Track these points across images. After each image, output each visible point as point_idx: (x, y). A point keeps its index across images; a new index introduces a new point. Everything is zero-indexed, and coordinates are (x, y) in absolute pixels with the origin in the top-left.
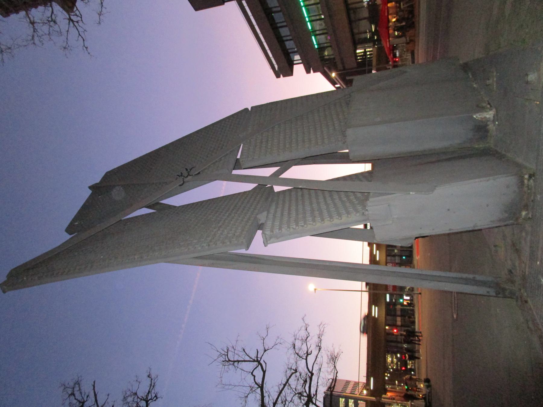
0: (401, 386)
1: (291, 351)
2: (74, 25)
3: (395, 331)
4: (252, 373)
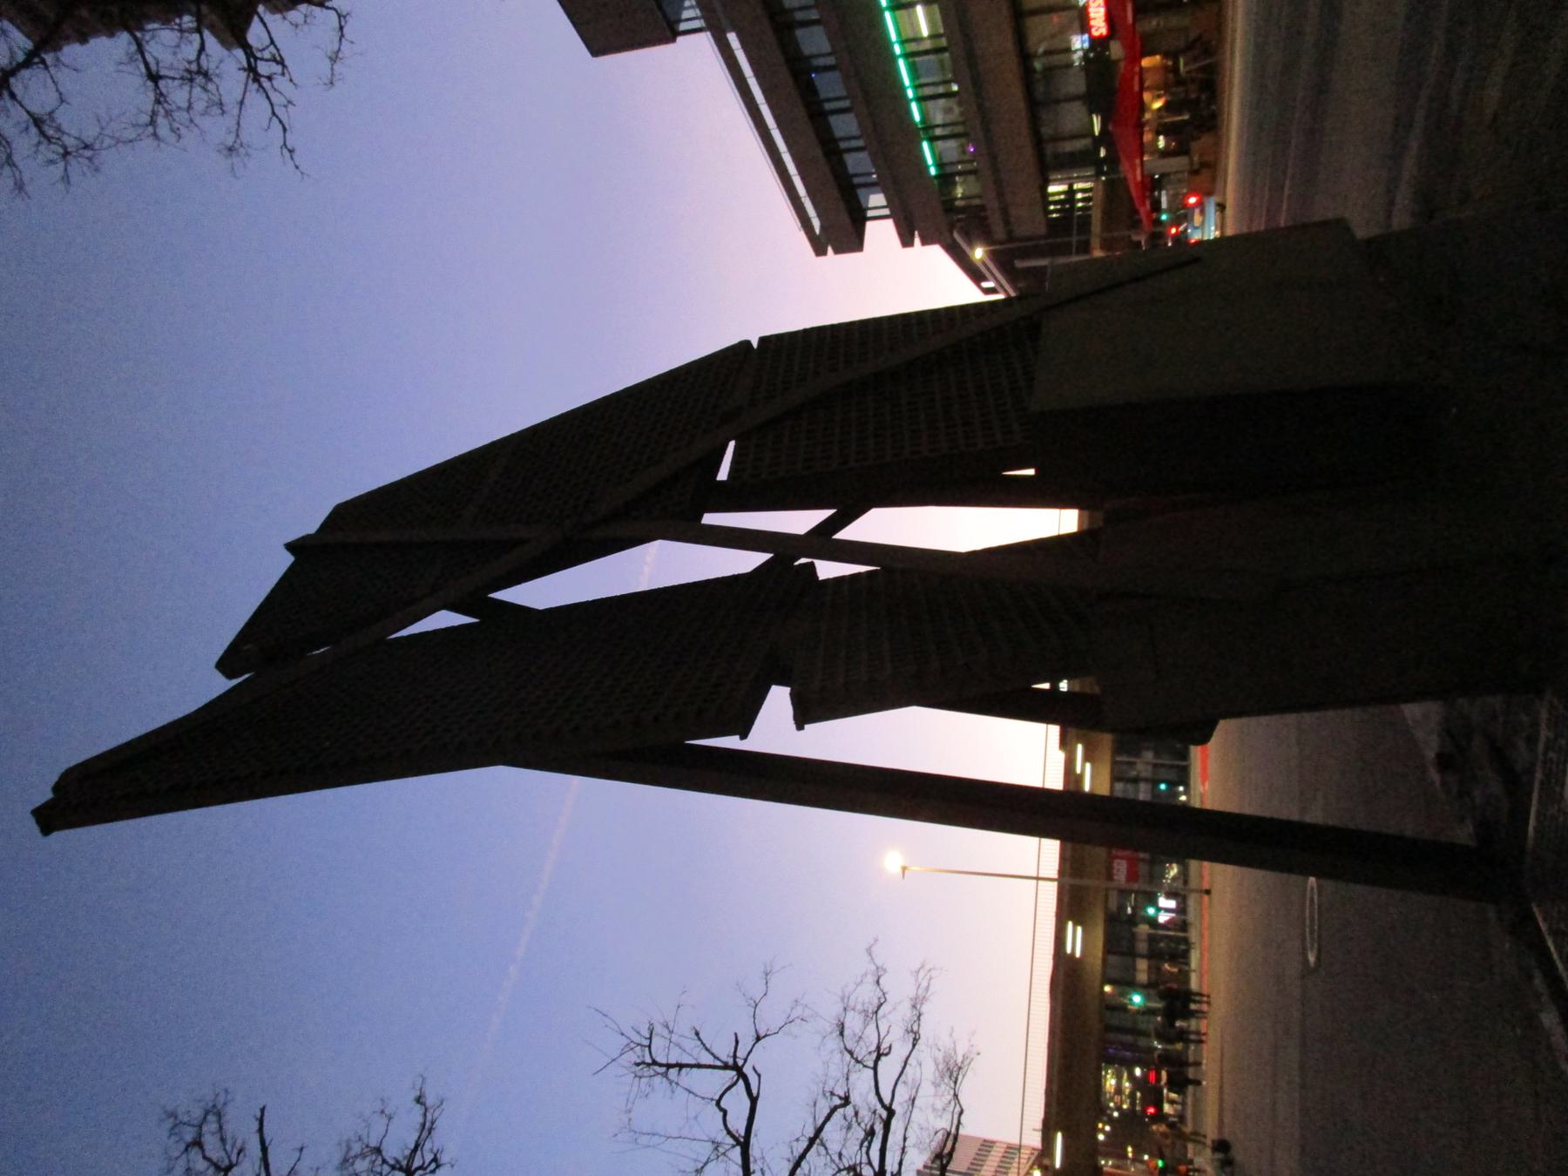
0: (1142, 1162)
1: (833, 1043)
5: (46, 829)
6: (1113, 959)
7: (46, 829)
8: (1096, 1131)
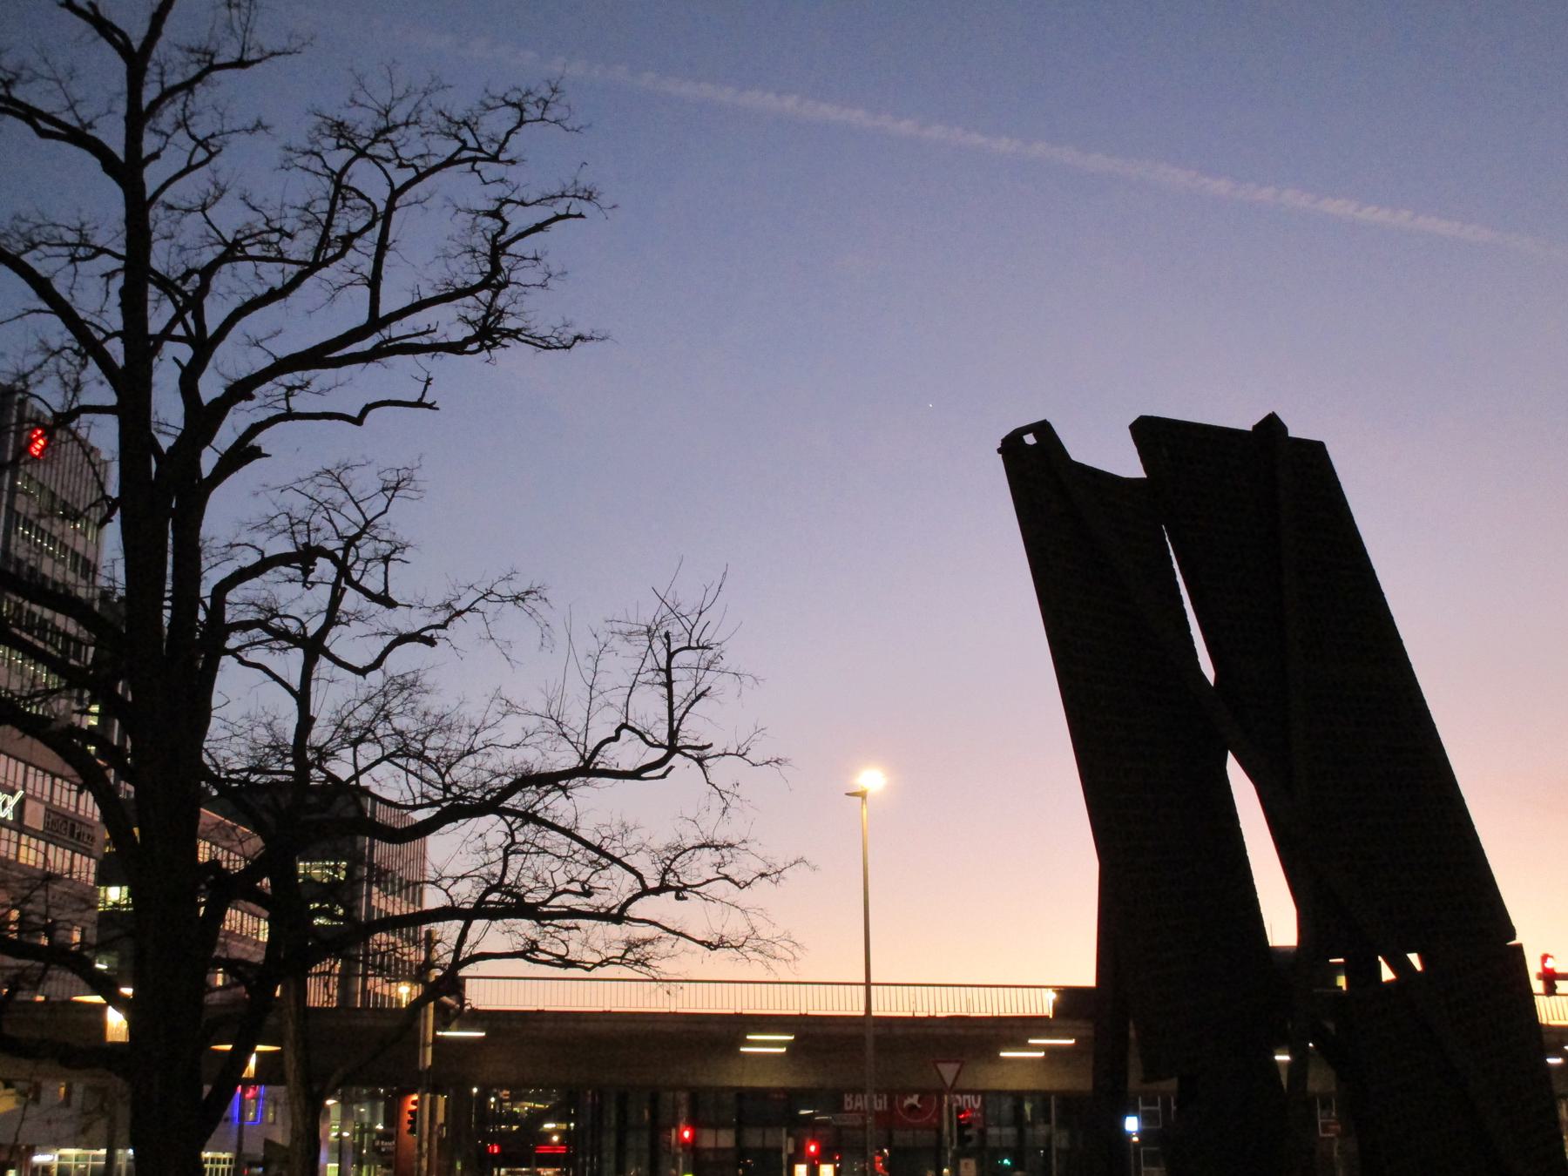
7: (1011, 447)
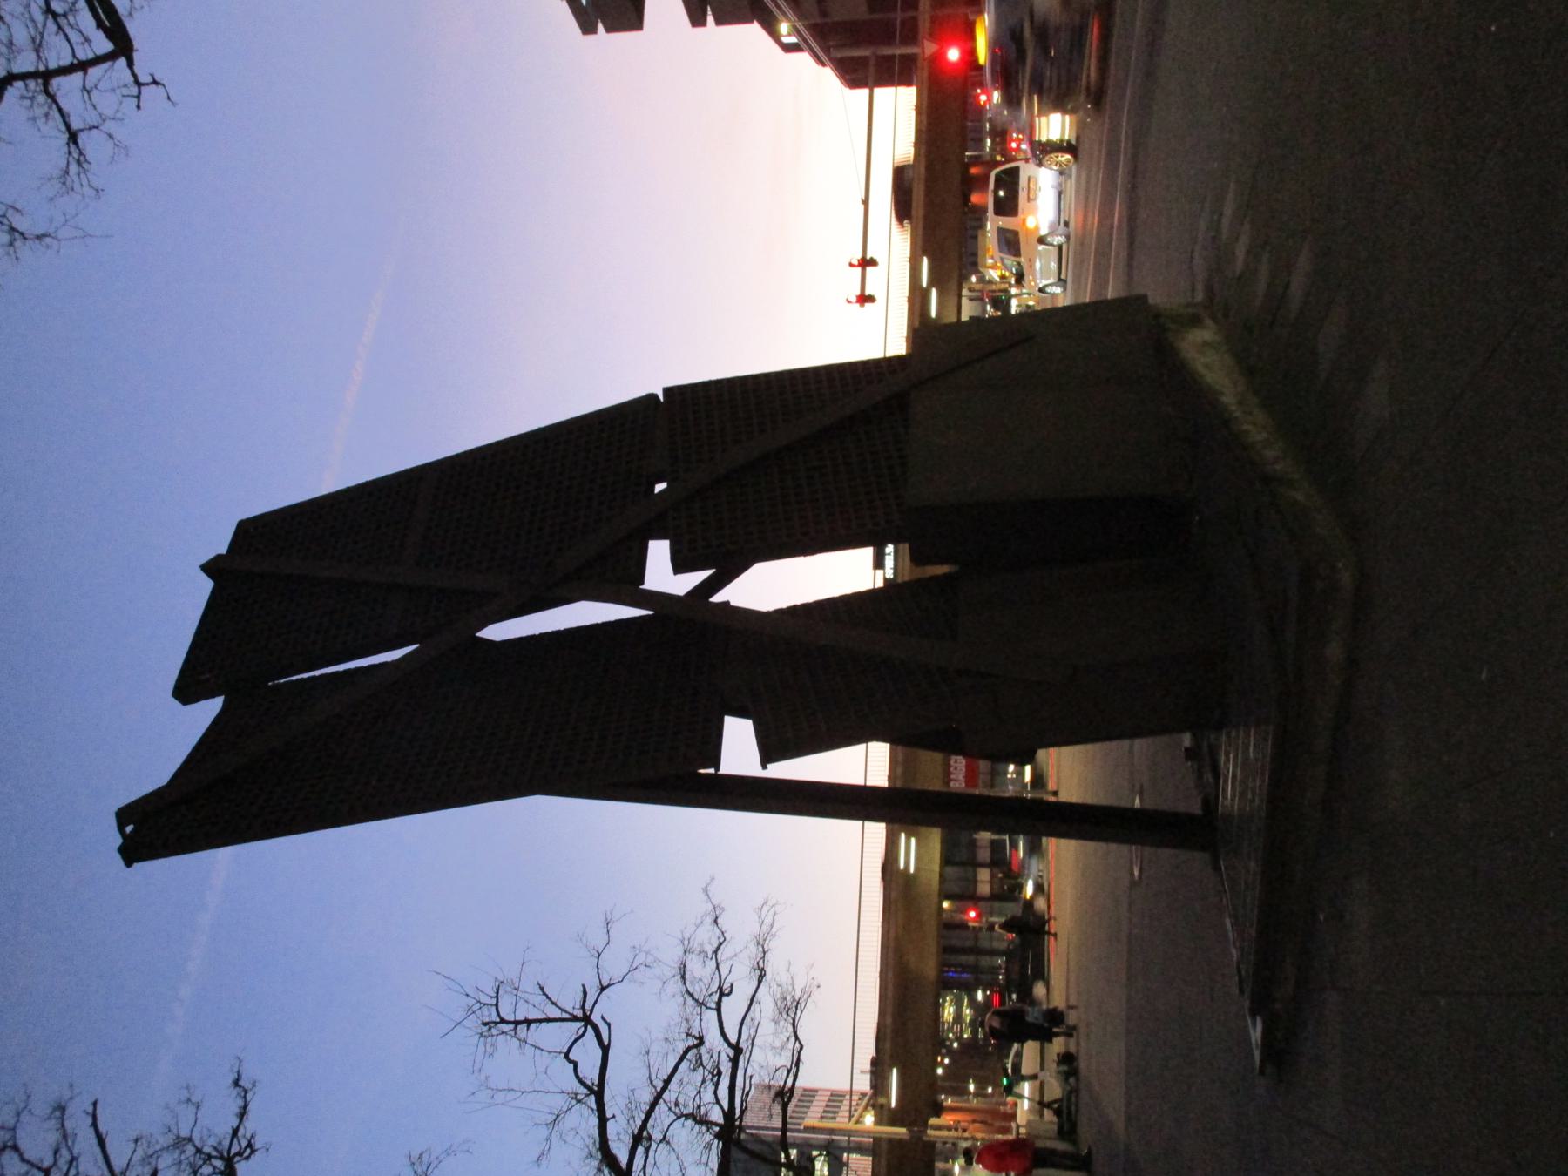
0: (986, 1096)
1: (675, 986)
2: (60, 28)
3: (972, 914)
4: (567, 1056)
5: (129, 863)
6: (949, 870)
8: (936, 1064)
